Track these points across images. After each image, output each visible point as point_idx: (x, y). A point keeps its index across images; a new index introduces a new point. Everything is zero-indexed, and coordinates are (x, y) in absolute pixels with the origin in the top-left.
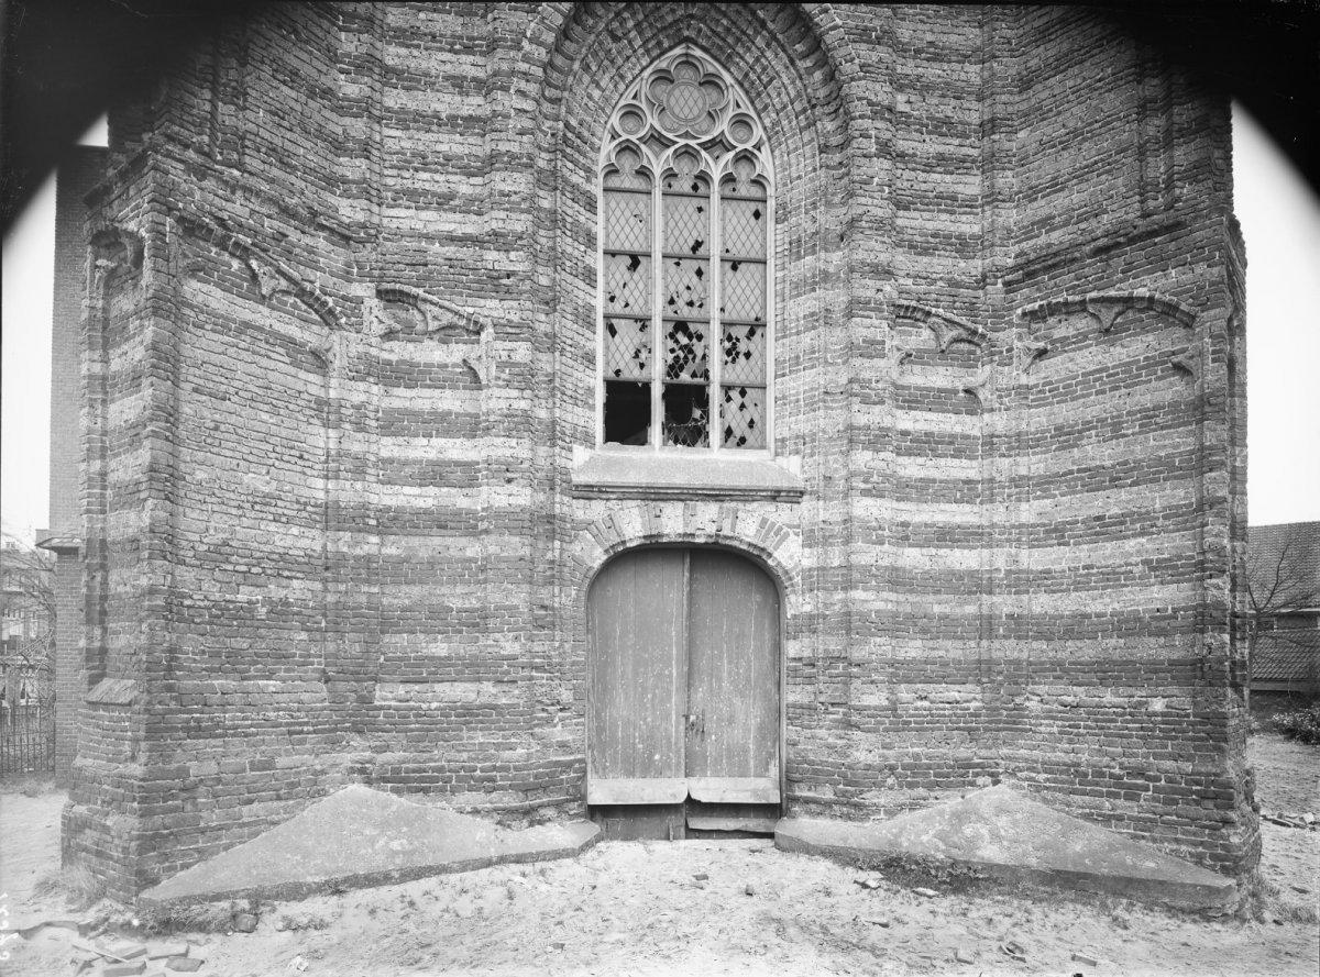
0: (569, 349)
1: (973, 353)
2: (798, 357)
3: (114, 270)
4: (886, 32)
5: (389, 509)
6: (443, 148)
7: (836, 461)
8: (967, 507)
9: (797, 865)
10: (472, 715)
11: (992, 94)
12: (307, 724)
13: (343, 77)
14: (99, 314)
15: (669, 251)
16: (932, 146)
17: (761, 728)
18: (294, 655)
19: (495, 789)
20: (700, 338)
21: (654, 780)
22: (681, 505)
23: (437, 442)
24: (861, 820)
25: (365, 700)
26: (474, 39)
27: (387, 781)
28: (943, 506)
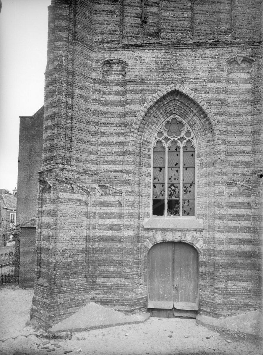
0: (143, 194)
1: (250, 192)
2: (202, 194)
3: (44, 188)
4: (224, 112)
5: (100, 236)
6: (114, 150)
7: (212, 221)
8: (248, 234)
9: (201, 328)
10: (119, 286)
11: (254, 124)
12: (82, 289)
13: (92, 136)
14: (41, 197)
15: (169, 166)
16: (238, 139)
17: (193, 289)
18: (79, 272)
19: (124, 305)
20: (177, 187)
21: (165, 302)
22: (171, 232)
23: (112, 220)
24: (217, 318)
25: (94, 282)
26: (121, 123)
27: (99, 302)
28: (241, 234)
